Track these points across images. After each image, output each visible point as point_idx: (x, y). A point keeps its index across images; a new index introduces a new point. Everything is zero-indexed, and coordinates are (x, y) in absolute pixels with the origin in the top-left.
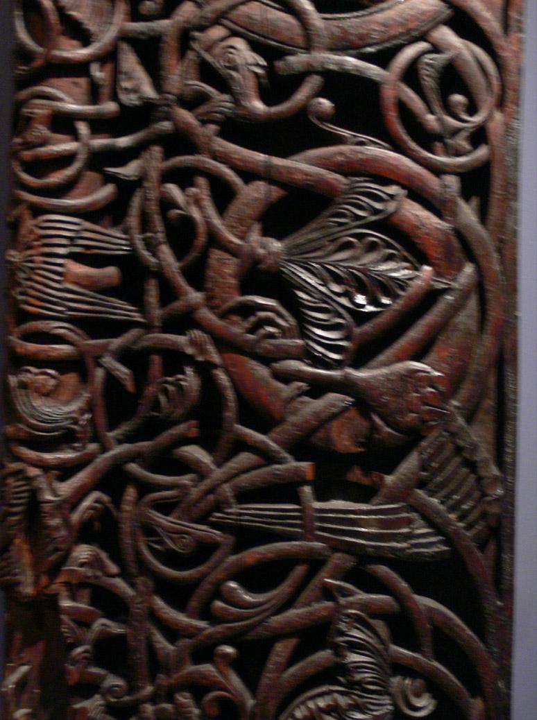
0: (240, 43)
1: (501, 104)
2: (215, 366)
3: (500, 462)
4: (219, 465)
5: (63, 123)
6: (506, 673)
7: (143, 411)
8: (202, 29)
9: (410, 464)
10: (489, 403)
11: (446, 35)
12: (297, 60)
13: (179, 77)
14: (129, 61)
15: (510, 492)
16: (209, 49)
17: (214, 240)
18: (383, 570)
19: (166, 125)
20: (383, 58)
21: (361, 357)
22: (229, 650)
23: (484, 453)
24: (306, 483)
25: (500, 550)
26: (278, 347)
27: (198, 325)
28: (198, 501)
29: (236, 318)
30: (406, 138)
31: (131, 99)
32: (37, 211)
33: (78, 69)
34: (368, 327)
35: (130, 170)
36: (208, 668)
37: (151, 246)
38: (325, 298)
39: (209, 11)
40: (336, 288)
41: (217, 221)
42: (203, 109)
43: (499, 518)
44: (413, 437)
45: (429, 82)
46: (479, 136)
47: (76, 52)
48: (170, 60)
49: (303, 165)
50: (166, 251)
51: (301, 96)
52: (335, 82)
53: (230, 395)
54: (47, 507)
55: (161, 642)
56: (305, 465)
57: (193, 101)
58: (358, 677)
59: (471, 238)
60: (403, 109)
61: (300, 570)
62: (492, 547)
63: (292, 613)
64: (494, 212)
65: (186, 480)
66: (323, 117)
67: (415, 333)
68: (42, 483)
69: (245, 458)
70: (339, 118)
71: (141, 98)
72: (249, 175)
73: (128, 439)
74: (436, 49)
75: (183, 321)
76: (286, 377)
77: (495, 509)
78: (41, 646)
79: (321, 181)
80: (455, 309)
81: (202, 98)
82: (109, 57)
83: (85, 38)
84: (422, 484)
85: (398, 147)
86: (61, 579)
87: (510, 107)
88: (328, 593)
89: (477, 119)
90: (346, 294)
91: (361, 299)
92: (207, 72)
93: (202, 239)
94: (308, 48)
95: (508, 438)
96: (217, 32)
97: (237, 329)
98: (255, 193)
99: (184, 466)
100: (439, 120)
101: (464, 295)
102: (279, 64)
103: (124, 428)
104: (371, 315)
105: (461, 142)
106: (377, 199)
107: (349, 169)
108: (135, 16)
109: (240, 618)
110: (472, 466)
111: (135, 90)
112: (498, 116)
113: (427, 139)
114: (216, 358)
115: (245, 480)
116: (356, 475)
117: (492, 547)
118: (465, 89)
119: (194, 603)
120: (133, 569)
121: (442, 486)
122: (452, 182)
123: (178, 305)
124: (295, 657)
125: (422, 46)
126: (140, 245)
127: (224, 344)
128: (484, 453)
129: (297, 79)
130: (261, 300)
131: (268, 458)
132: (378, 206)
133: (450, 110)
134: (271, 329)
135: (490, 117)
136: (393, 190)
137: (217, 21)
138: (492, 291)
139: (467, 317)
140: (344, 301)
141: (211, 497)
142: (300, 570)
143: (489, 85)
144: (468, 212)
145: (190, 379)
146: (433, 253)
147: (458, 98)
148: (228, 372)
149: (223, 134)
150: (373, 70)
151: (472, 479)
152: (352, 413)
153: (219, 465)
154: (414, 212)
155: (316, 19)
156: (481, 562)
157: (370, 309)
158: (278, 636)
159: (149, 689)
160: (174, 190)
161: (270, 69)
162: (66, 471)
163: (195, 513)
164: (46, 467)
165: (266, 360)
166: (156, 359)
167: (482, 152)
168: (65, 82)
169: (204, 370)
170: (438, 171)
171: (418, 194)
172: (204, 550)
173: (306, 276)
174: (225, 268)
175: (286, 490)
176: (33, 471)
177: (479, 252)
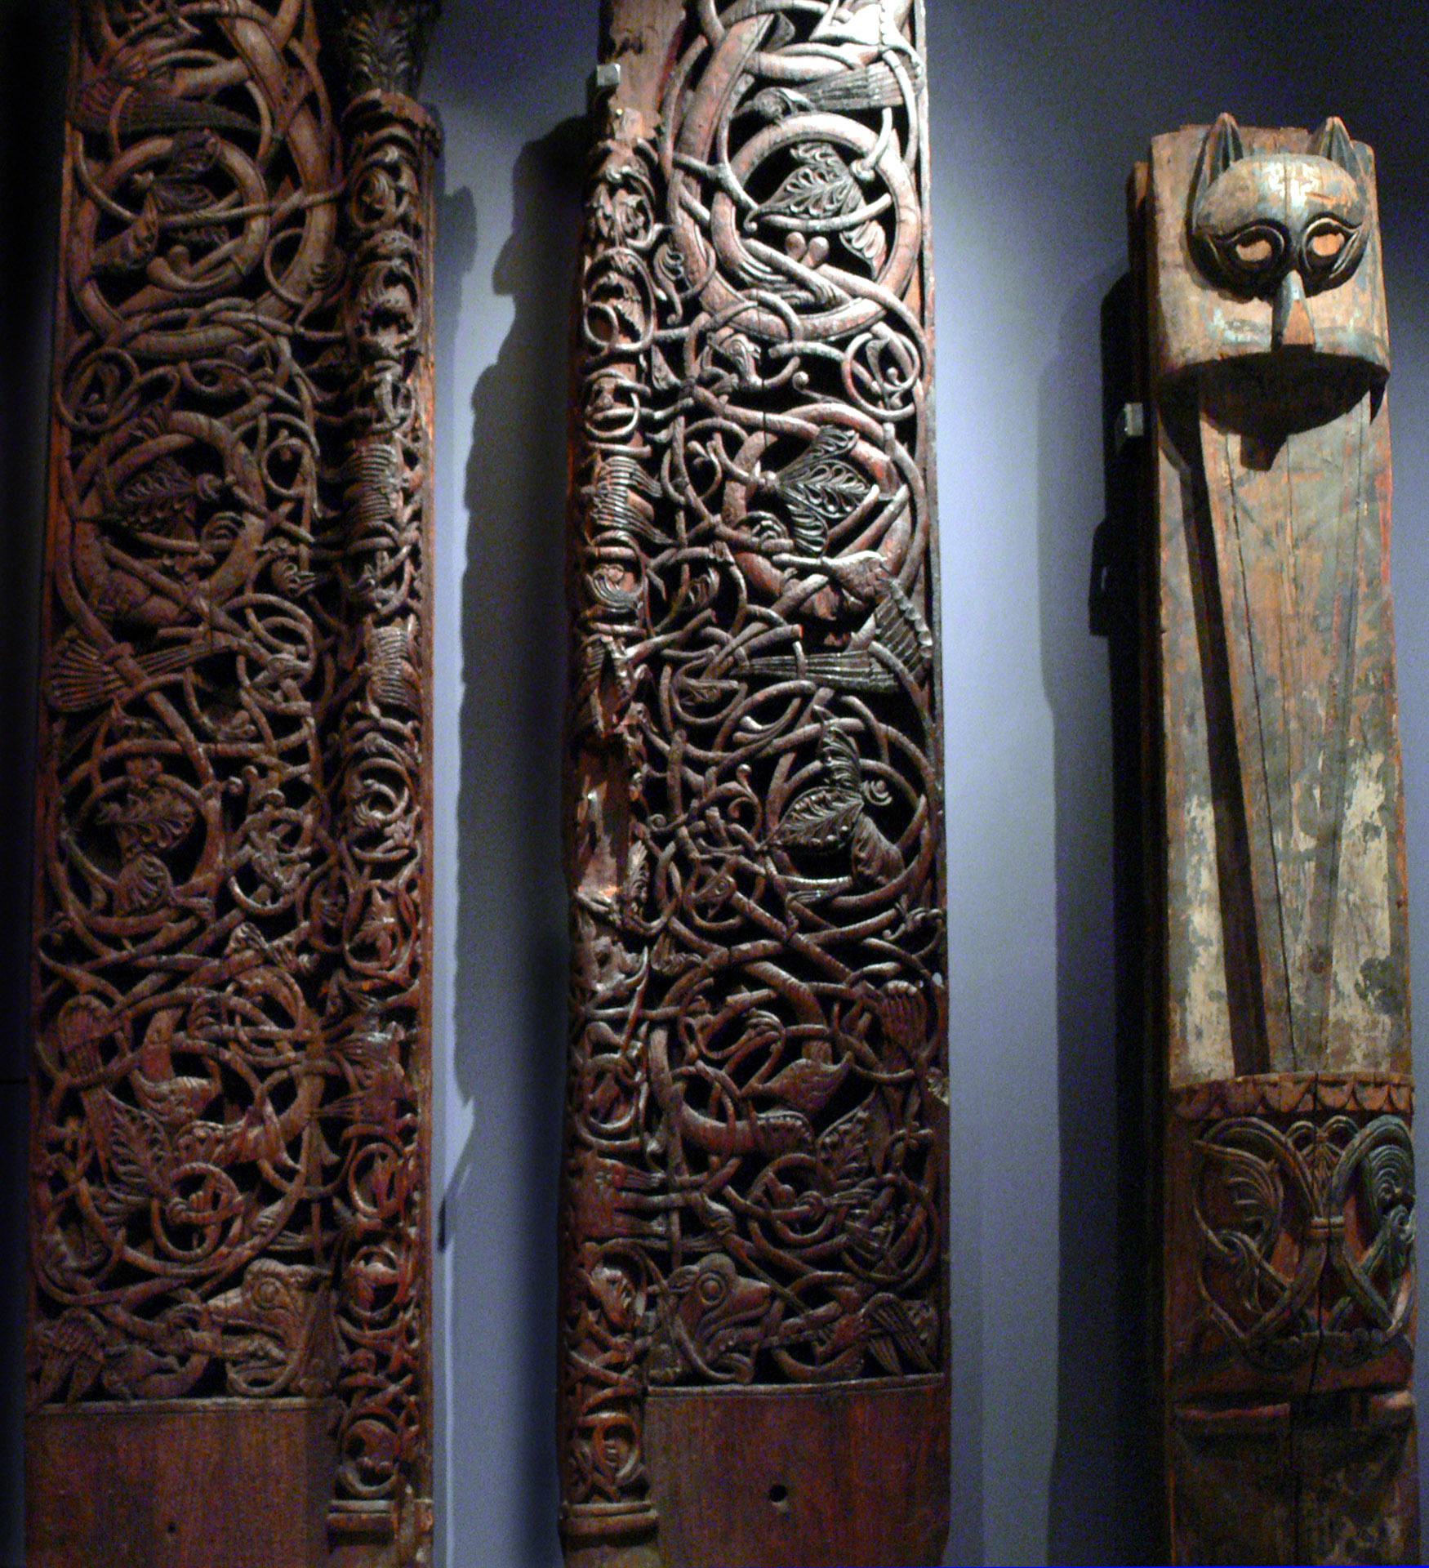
0: (742, 338)
1: (921, 375)
2: (731, 564)
3: (930, 623)
4: (735, 636)
5: (622, 395)
6: (940, 775)
7: (676, 607)
8: (715, 330)
9: (870, 623)
10: (919, 587)
11: (882, 328)
12: (785, 347)
13: (695, 367)
14: (659, 359)
15: (937, 642)
16: (721, 344)
17: (729, 475)
18: (855, 701)
19: (690, 401)
20: (842, 344)
21: (834, 549)
22: (745, 767)
23: (917, 616)
24: (797, 639)
25: (932, 686)
26: (776, 545)
27: (721, 538)
28: (721, 662)
29: (745, 528)
30: (859, 397)
31: (662, 385)
32: (606, 455)
33: (629, 358)
34: (837, 529)
35: (662, 436)
36: (733, 785)
37: (680, 489)
38: (809, 509)
39: (719, 317)
40: (816, 501)
41: (729, 462)
42: (716, 386)
43: (930, 661)
44: (870, 604)
45: (872, 360)
46: (908, 397)
47: (626, 345)
48: (689, 354)
49: (791, 419)
50: (690, 491)
51: (787, 371)
52: (810, 362)
53: (742, 582)
54: (618, 663)
55: (695, 778)
56: (797, 627)
57: (709, 382)
58: (837, 777)
59: (905, 465)
60: (857, 380)
61: (796, 702)
62: (927, 687)
63: (792, 736)
64: (919, 448)
65: (712, 650)
66: (802, 386)
67: (869, 532)
68: (613, 647)
69: (756, 627)
70: (813, 385)
71: (669, 384)
72: (751, 428)
73: (664, 632)
74: (876, 337)
75: (708, 537)
76: (782, 566)
77: (927, 655)
78: (604, 786)
79: (802, 429)
80: (894, 517)
81: (716, 378)
82: (648, 354)
83: (634, 335)
84: (877, 638)
85: (852, 402)
86: (625, 722)
87: (927, 377)
88: (816, 717)
89: (906, 385)
90: (822, 505)
91: (831, 508)
92: (719, 360)
93: (719, 475)
94: (790, 338)
95: (935, 604)
96: (726, 332)
97: (745, 535)
98: (757, 442)
99: (711, 641)
100: (881, 387)
101: (902, 506)
102: (770, 351)
103: (658, 628)
104: (838, 521)
105: (896, 400)
106: (841, 439)
107: (821, 420)
108: (662, 325)
109: (754, 741)
110: (911, 625)
111: (665, 378)
112: (919, 383)
113: (874, 398)
114: (731, 559)
115: (754, 642)
116: (830, 640)
117: (927, 687)
118: (897, 365)
119: (719, 739)
120: (669, 727)
121: (890, 639)
122: (890, 428)
123: (703, 525)
124: (795, 768)
125: (867, 336)
126: (671, 489)
127: (737, 547)
128: (917, 616)
129: (783, 361)
130: (763, 514)
131: (771, 623)
132: (842, 444)
133: (887, 379)
134: (771, 533)
135: (914, 383)
136: (851, 433)
137: (725, 324)
138: (920, 502)
139: (902, 524)
140: (820, 510)
141: (730, 659)
142: (796, 702)
143: (913, 362)
144: (902, 450)
145: (714, 577)
146: (881, 475)
147: (892, 371)
148: (740, 568)
149: (732, 402)
150: (835, 353)
151: (911, 635)
152: (828, 589)
153: (735, 636)
154: (864, 449)
155: (794, 318)
156: (920, 696)
157: (837, 516)
158: (781, 753)
159: (683, 817)
160: (696, 445)
161: (764, 354)
162: (631, 640)
163: (718, 672)
164: (616, 635)
165: (768, 555)
166: (686, 568)
167: (909, 409)
168: (623, 366)
169: (723, 568)
170: (881, 421)
171: (867, 436)
172: (728, 696)
173: (793, 494)
174: (737, 495)
175: (784, 646)
176: (606, 639)
177: (910, 476)
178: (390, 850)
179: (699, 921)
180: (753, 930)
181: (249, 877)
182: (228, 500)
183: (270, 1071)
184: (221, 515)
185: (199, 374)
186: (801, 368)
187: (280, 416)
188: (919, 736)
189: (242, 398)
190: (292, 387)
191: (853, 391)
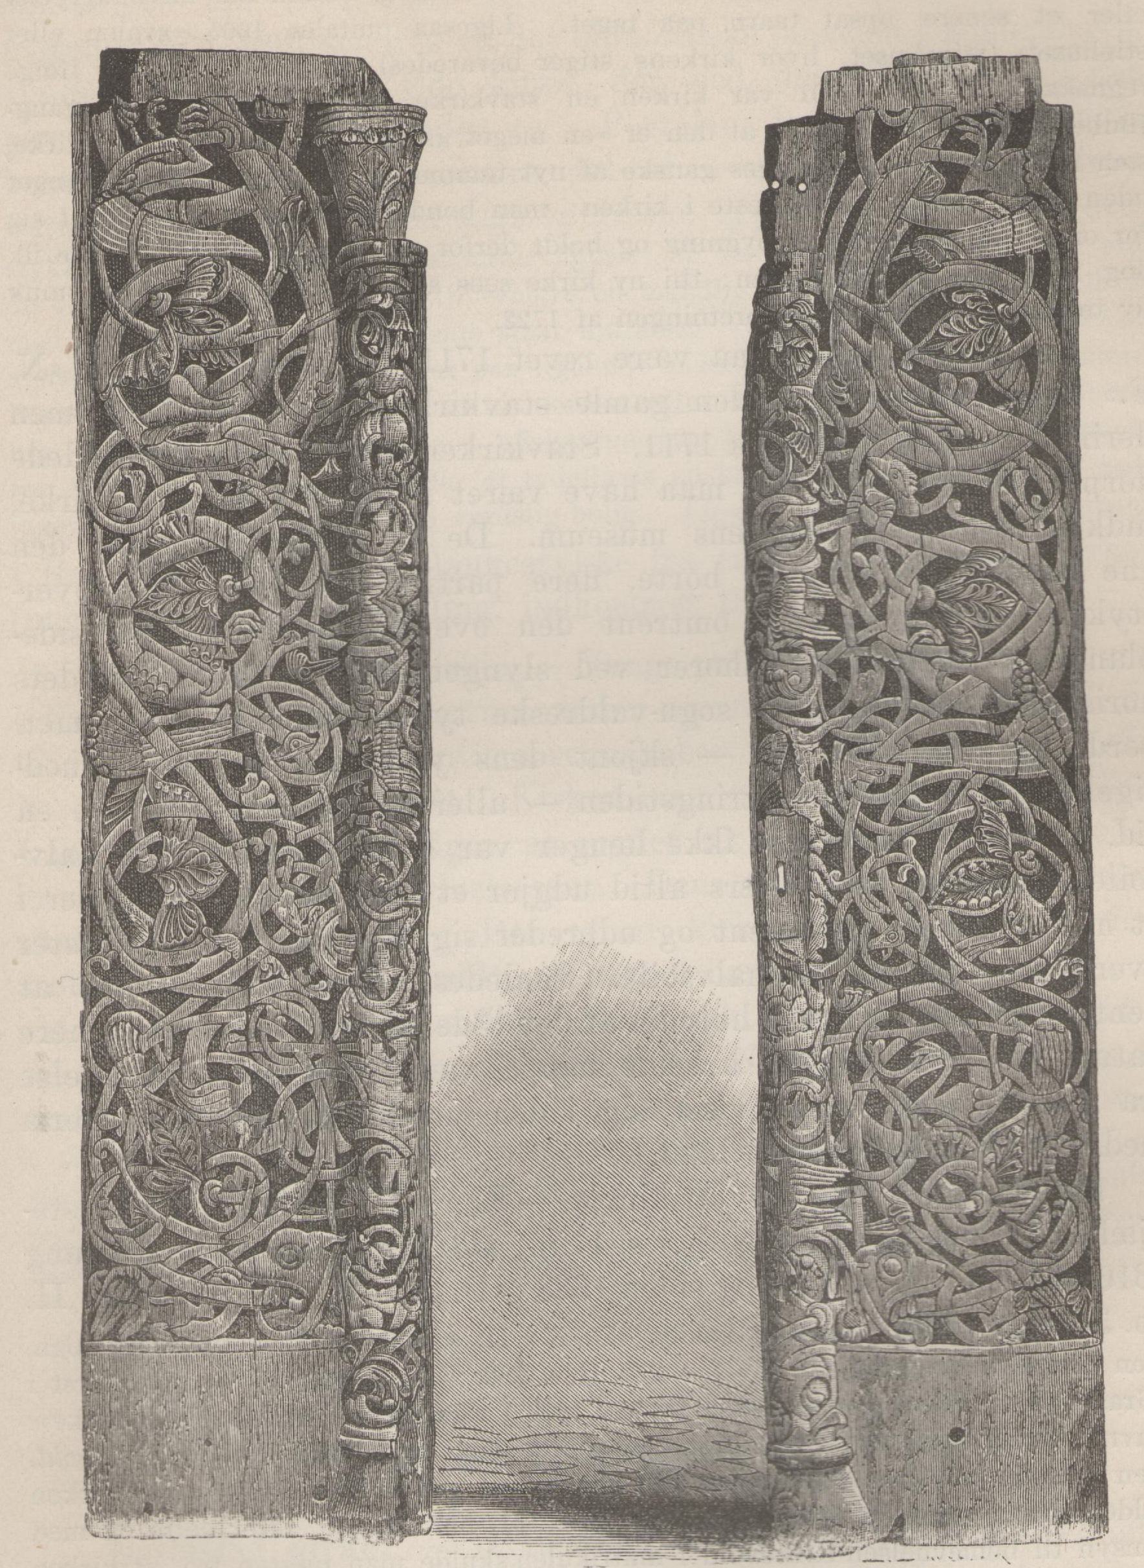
52: (961, 491)
98: (913, 562)
118: (1040, 491)
129: (936, 489)
178: (846, 930)
179: (881, 969)
180: (920, 975)
181: (270, 921)
182: (246, 600)
183: (291, 1077)
184: (237, 613)
185: (219, 485)
186: (954, 495)
187: (288, 523)
188: (1060, 811)
189: (258, 509)
190: (300, 497)
191: (1000, 516)
